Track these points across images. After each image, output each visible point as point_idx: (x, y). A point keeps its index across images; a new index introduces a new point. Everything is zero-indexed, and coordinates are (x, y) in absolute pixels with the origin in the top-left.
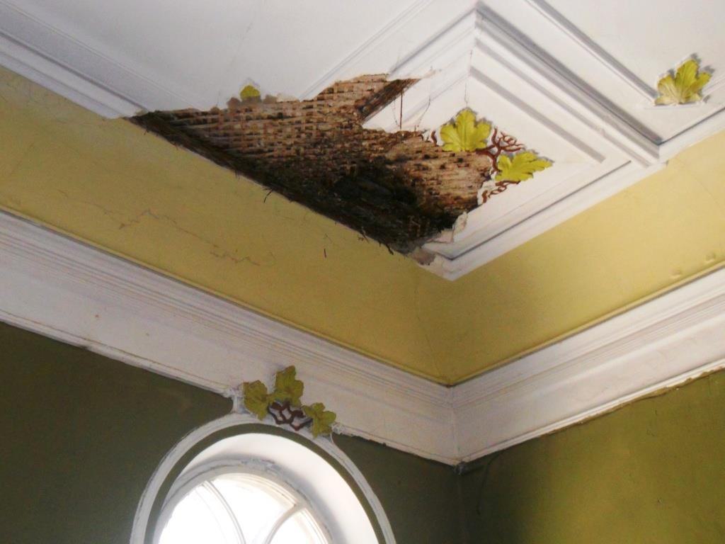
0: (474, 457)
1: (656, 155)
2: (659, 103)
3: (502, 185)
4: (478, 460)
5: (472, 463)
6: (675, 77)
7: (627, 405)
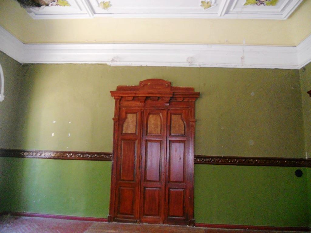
0: (27, 63)
1: (93, 16)
2: (99, 6)
3: (57, 5)
4: (28, 64)
5: (26, 64)
6: (104, 3)
7: (67, 64)
